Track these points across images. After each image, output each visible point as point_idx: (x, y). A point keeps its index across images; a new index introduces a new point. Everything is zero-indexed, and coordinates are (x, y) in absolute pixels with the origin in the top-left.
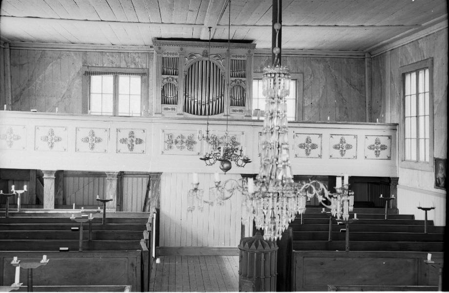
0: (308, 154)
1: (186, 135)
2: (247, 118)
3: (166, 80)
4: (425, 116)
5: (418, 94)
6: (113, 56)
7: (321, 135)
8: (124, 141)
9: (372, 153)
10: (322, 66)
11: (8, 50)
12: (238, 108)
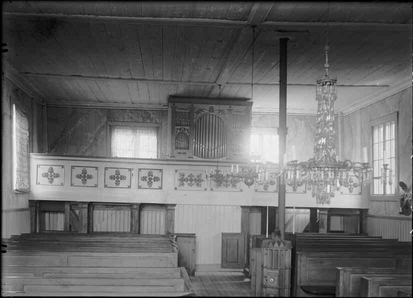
0: (295, 190)
1: (195, 174)
2: (172, 158)
3: (179, 131)
4: (391, 158)
5: (384, 141)
6: (132, 113)
7: (97, 168)
8: (144, 179)
9: (202, 186)
10: (303, 122)
12: (182, 151)
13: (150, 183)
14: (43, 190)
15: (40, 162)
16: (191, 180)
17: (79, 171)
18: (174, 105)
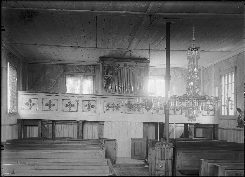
3: (106, 78)
5: (228, 84)
7: (57, 100)
8: (85, 106)
10: (180, 73)
11: (27, 63)
13: (89, 109)
14: (25, 113)
15: (24, 96)
16: (113, 107)
17: (47, 102)
18: (103, 62)
